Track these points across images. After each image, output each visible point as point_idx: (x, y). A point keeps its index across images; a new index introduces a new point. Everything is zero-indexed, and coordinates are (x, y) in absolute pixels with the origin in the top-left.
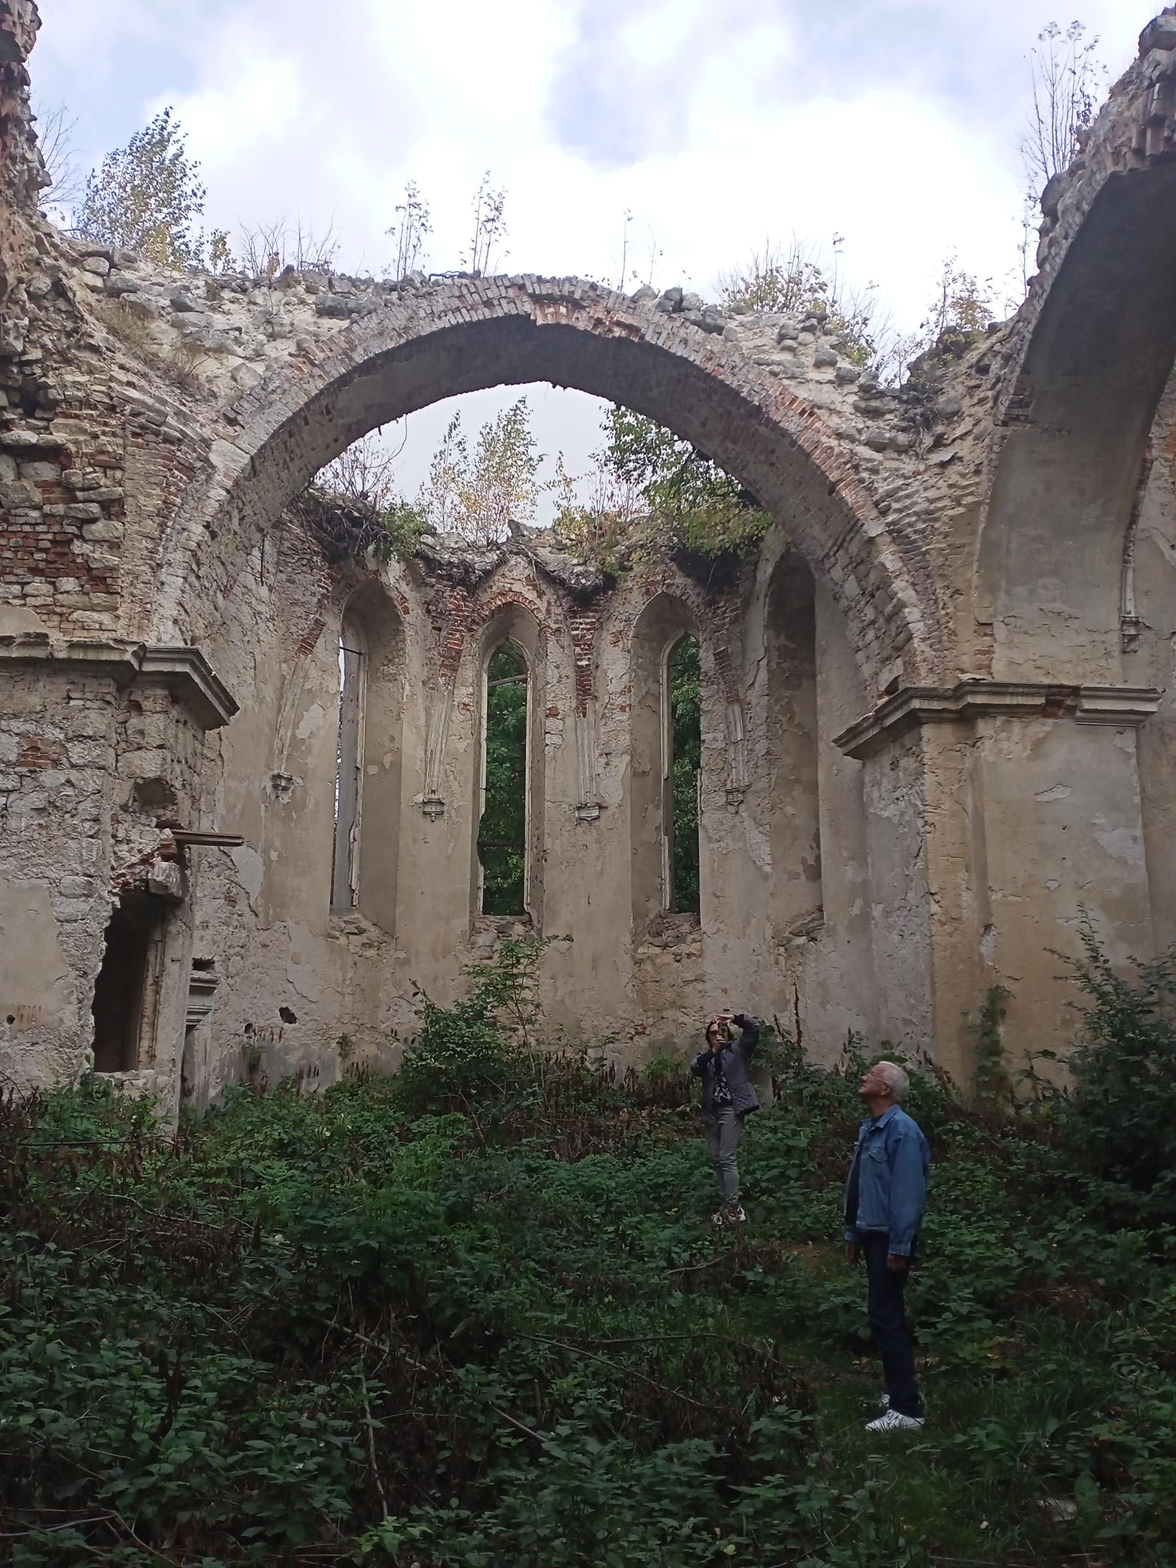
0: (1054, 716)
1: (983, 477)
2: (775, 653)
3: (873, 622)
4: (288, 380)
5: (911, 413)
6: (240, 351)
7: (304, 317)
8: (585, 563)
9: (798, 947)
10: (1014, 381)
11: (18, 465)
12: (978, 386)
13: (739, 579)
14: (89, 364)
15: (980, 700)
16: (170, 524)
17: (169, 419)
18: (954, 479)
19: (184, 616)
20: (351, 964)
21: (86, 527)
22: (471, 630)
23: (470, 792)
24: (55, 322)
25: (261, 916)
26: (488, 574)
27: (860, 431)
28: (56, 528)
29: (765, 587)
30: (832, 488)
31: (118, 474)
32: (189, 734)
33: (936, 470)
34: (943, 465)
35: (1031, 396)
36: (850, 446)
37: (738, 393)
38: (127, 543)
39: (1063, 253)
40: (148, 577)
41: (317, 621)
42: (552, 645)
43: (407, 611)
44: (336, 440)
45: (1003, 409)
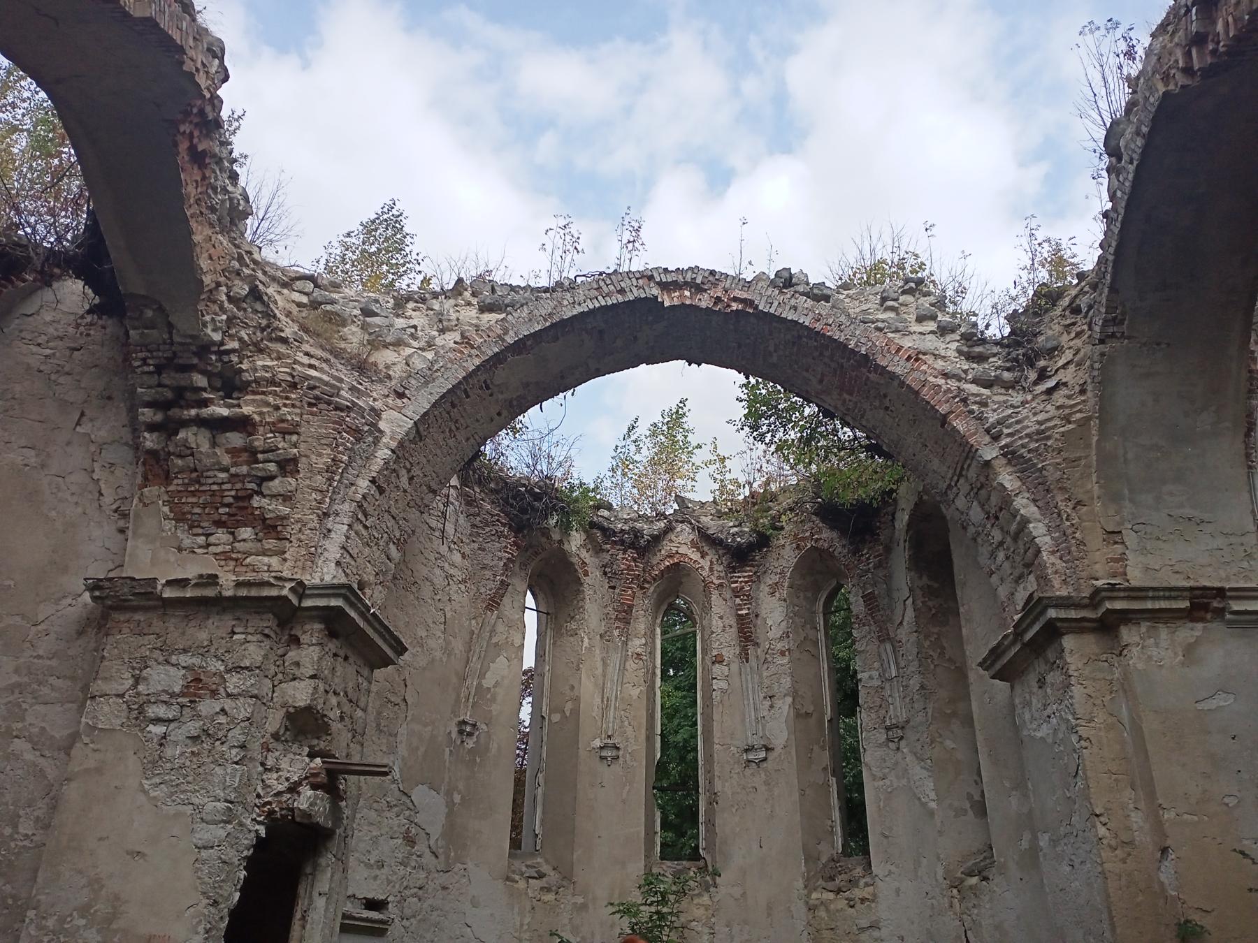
0: (1202, 620)
1: (1089, 394)
2: (919, 592)
3: (1001, 544)
4: (451, 361)
5: (1014, 355)
6: (415, 344)
7: (469, 314)
8: (740, 525)
9: (971, 887)
10: (1104, 301)
11: (214, 437)
12: (1074, 324)
13: (879, 528)
14: (278, 352)
15: (1119, 605)
16: (337, 478)
17: (343, 393)
18: (1061, 401)
19: (348, 559)
20: (528, 908)
21: (265, 484)
22: (643, 588)
23: (643, 737)
24: (252, 320)
25: (442, 858)
26: (657, 539)
27: (965, 372)
28: (239, 486)
29: (903, 533)
30: (944, 420)
31: (294, 438)
32: (351, 670)
33: (1044, 397)
34: (1050, 392)
35: (1123, 313)
36: (957, 384)
37: (846, 346)
38: (299, 496)
39: (1131, 177)
40: (316, 524)
41: (503, 582)
42: (715, 598)
43: (586, 574)
44: (499, 414)
45: (1097, 329)
